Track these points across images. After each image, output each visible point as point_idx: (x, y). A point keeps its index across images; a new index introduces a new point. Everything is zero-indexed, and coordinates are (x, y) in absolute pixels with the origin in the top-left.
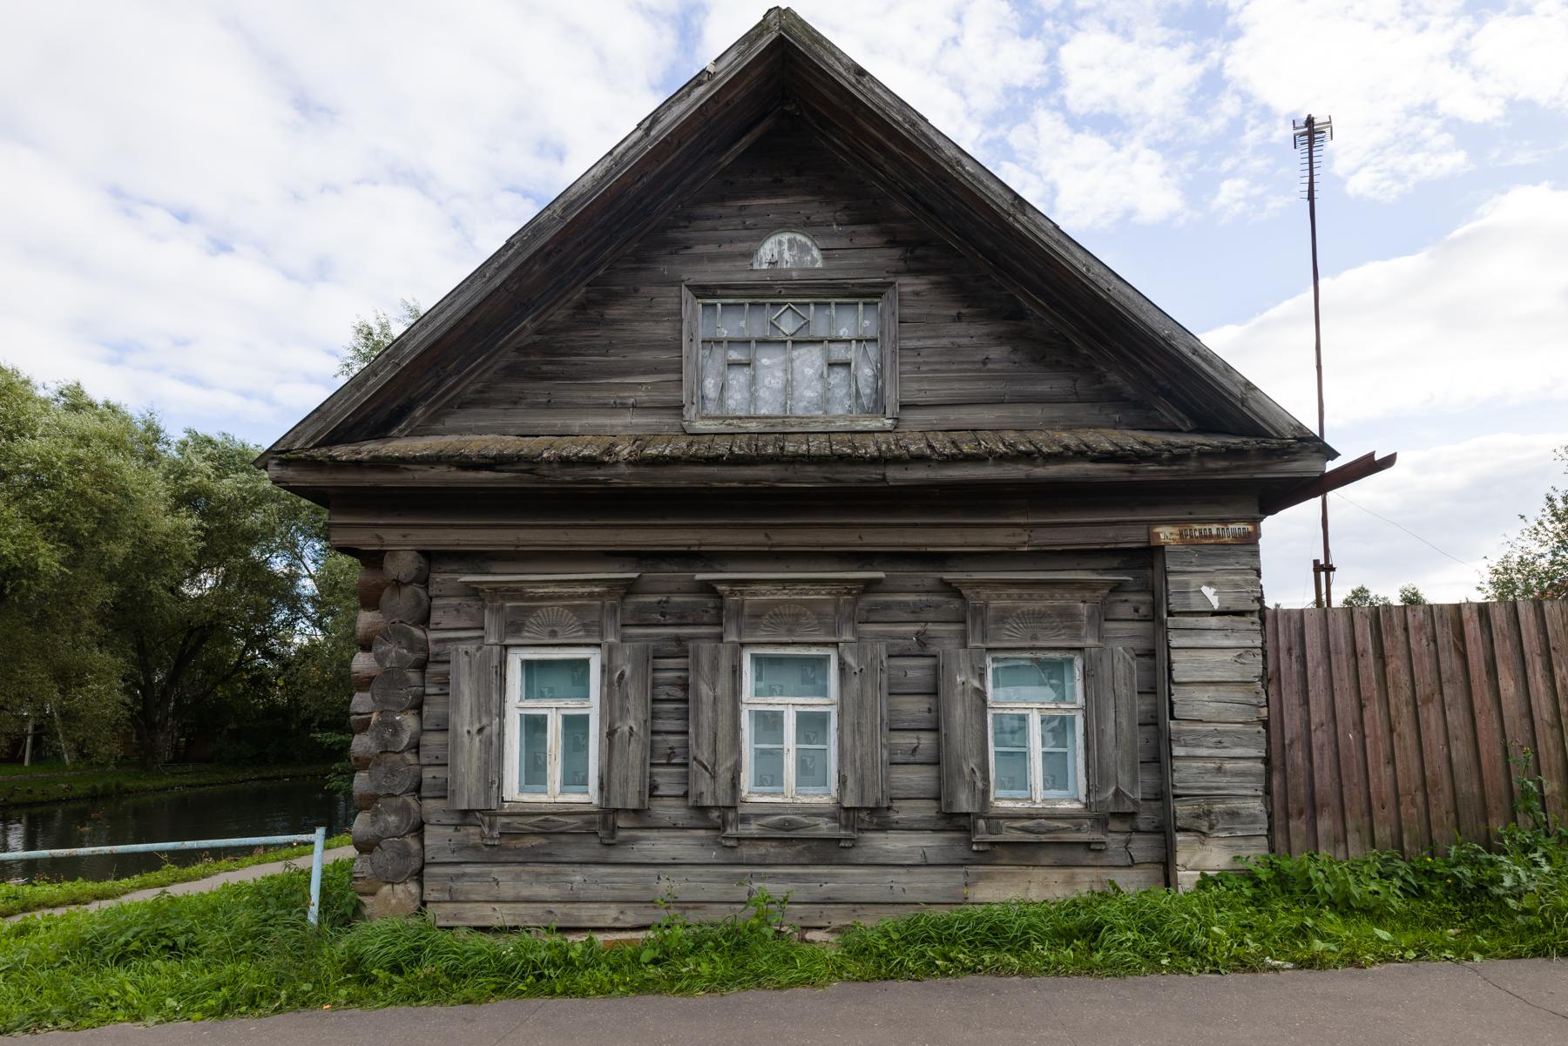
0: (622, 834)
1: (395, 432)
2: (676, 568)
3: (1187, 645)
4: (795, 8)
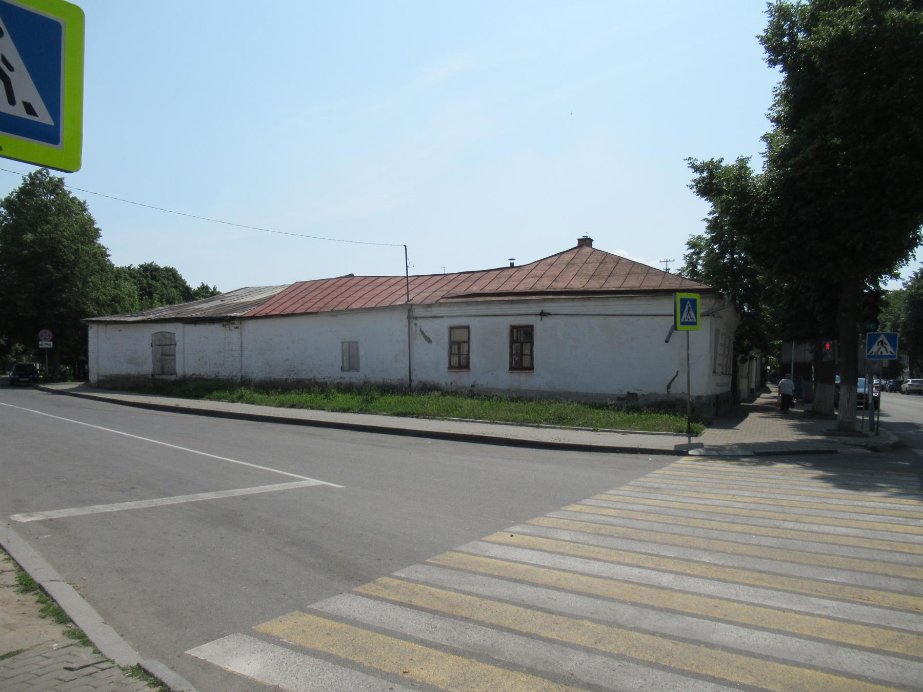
0: (60, 267)
3: (494, 318)
4: (32, 104)
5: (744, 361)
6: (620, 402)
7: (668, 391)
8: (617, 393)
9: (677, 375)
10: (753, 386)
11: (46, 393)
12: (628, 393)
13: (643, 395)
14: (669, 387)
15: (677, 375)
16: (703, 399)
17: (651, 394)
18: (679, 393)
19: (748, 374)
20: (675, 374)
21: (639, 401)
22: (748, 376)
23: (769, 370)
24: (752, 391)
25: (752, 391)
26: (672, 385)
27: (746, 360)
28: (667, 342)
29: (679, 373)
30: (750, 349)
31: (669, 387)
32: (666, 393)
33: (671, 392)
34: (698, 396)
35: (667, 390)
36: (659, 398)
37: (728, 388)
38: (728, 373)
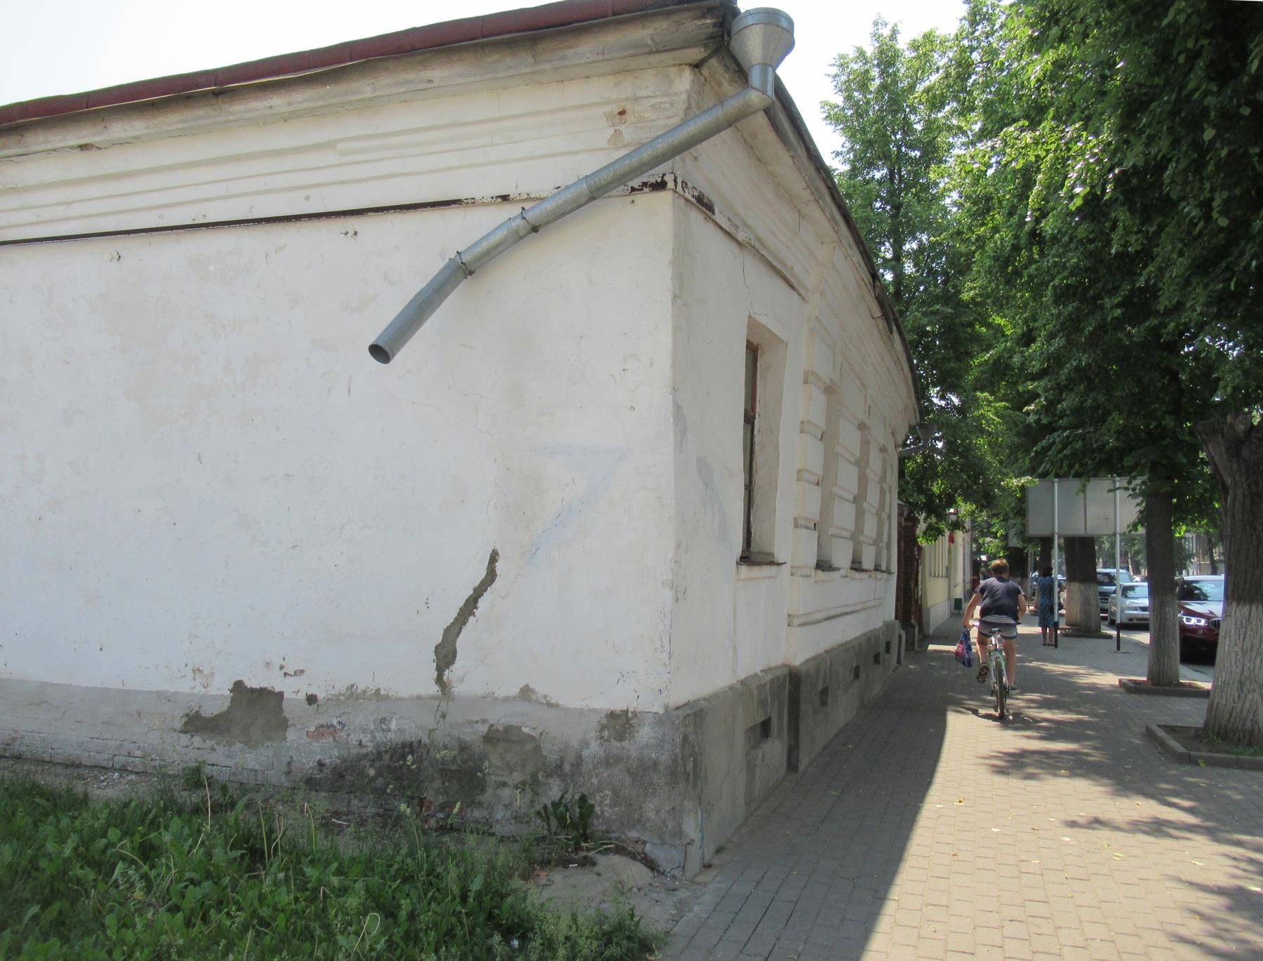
1: (1141, 530)
2: (604, 175)
5: (933, 532)
6: (197, 741)
7: (439, 680)
8: (186, 686)
9: (491, 576)
10: (959, 593)
11: (920, 575)
12: (238, 687)
13: (311, 699)
14: (445, 655)
15: (491, 576)
16: (645, 734)
17: (353, 696)
18: (500, 693)
19: (948, 569)
20: (483, 573)
21: (291, 735)
22: (948, 574)
23: (984, 562)
24: (958, 604)
25: (958, 604)
26: (463, 642)
27: (940, 532)
28: (380, 352)
29: (499, 566)
30: (951, 501)
31: (445, 655)
32: (434, 689)
33: (458, 689)
34: (612, 715)
35: (440, 670)
36: (394, 725)
37: (889, 611)
38: (868, 563)
